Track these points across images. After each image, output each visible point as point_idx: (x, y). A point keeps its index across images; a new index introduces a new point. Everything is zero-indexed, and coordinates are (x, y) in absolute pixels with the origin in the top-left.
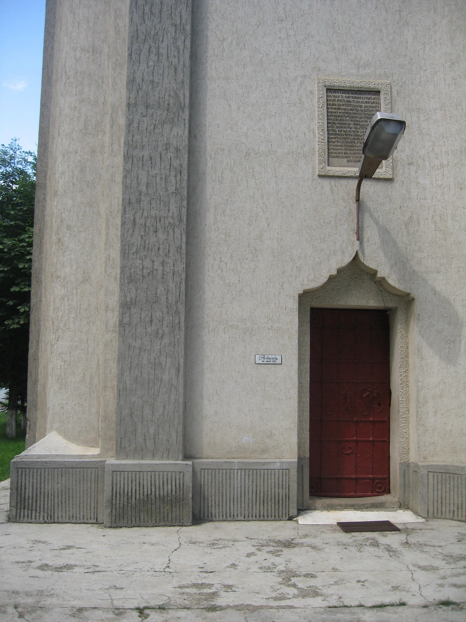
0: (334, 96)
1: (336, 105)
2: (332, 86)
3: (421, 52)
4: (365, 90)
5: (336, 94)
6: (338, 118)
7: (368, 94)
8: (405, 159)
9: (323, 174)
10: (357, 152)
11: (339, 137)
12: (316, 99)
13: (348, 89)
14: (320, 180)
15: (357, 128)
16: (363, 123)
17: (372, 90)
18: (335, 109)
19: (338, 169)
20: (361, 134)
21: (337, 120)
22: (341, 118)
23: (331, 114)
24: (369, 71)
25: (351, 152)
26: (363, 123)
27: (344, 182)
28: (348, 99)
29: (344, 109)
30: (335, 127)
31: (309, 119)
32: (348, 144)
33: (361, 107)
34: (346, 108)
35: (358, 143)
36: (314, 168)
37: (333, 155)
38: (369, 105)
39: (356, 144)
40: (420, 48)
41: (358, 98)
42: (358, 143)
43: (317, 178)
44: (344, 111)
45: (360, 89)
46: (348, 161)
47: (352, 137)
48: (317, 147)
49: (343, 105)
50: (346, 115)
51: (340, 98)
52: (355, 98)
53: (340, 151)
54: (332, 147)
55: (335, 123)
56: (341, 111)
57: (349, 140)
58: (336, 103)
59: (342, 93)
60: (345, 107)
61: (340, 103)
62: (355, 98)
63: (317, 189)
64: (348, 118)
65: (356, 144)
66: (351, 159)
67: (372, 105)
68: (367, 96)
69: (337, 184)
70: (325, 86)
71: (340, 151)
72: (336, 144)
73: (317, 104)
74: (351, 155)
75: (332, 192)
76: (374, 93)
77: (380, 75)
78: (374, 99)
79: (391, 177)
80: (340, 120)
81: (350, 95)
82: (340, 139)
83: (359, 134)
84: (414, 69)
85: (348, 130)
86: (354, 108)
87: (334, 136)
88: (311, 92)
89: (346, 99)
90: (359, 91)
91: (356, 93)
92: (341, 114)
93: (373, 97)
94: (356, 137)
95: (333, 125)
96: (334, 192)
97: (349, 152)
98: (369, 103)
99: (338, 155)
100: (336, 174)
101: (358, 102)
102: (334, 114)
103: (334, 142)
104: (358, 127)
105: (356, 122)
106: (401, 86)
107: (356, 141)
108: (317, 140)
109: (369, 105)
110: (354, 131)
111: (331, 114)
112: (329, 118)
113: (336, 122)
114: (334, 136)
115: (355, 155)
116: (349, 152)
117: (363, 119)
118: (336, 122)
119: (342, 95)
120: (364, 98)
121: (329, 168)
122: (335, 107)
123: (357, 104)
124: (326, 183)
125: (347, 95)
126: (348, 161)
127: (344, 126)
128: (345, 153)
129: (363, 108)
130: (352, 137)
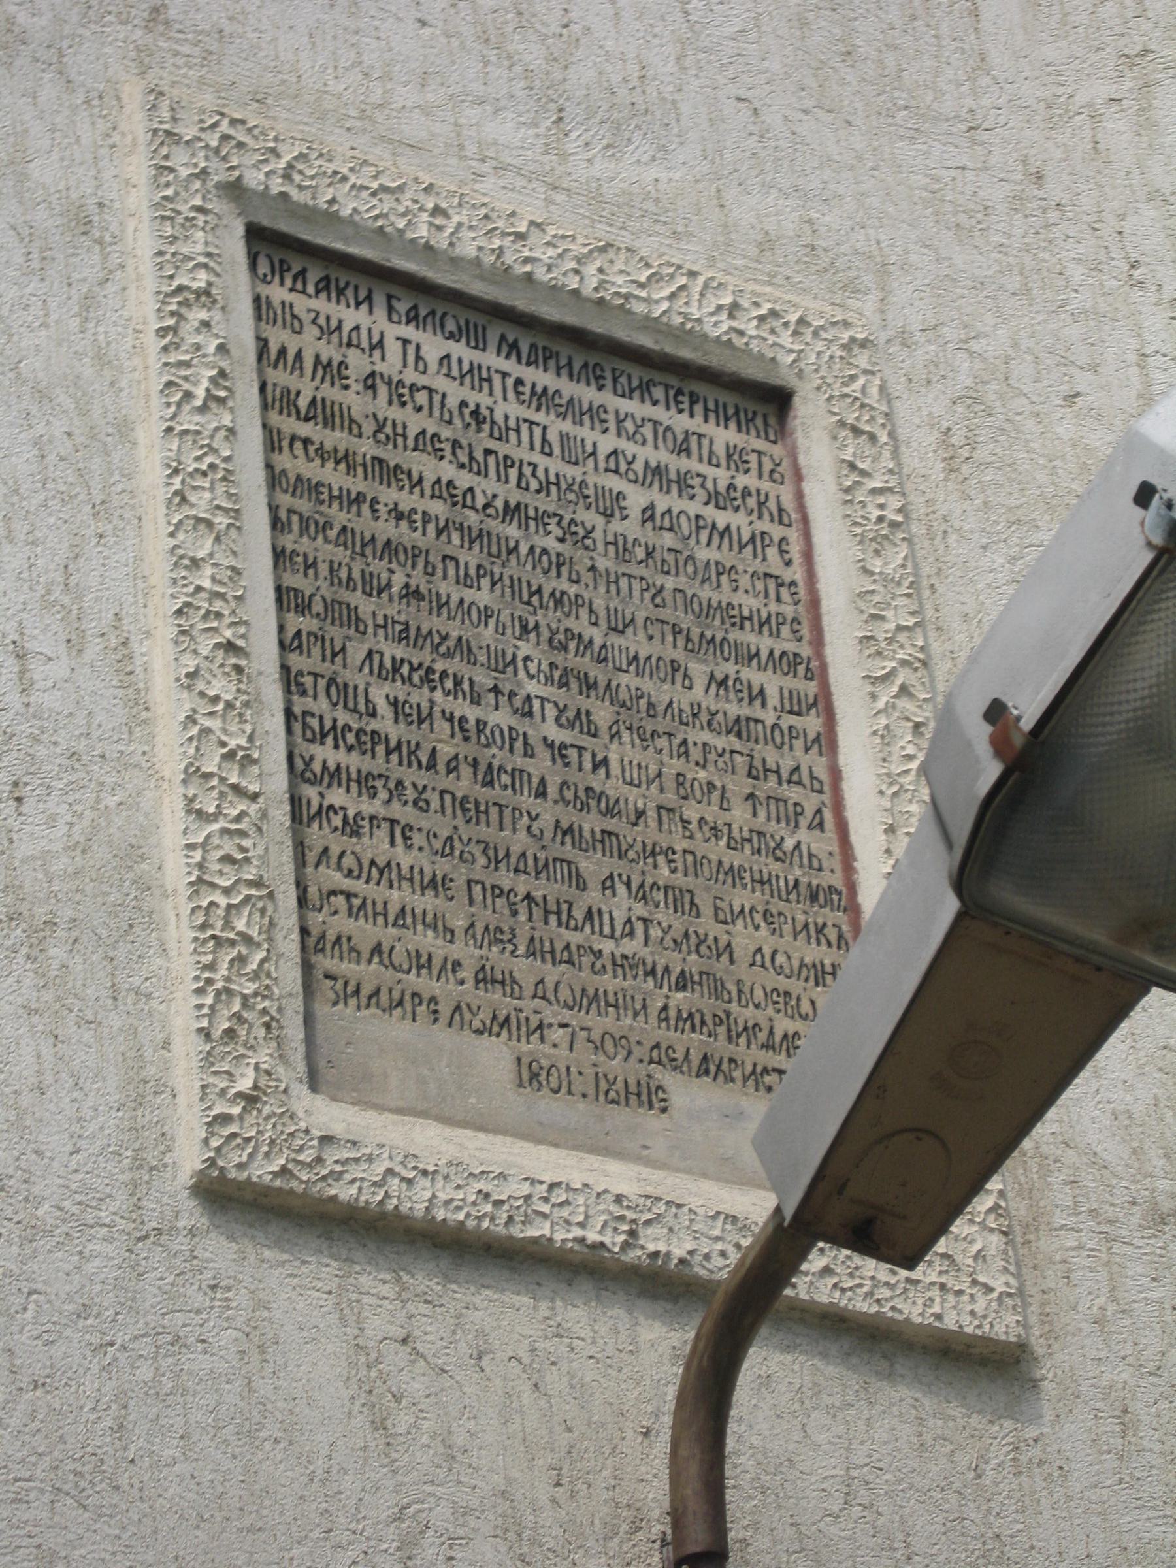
0: (329, 330)
1: (352, 425)
2: (309, 214)
3: (1117, 129)
4: (645, 341)
5: (352, 316)
6: (379, 567)
7: (674, 399)
8: (1113, 1151)
9: (263, 1171)
10: (609, 983)
11: (412, 776)
12: (142, 304)
13: (477, 288)
14: (221, 1251)
15: (581, 720)
16: (647, 685)
17: (714, 359)
18: (345, 459)
19: (431, 1141)
20: (634, 798)
21: (375, 588)
22: (418, 579)
23: (304, 505)
24: (653, 172)
25: (553, 973)
26: (647, 685)
27: (508, 1315)
28: (473, 398)
29: (445, 490)
30: (357, 652)
31: (67, 499)
32: (505, 879)
33: (612, 507)
34: (464, 479)
35: (608, 884)
36: (143, 1091)
37: (346, 968)
38: (693, 508)
39: (593, 896)
40: (1106, 90)
41: (571, 410)
42: (608, 884)
43: (191, 1214)
44: (438, 508)
45: (596, 325)
46: (531, 1075)
47: (548, 814)
48: (172, 832)
49: (427, 442)
50: (471, 558)
51: (391, 363)
52: (542, 398)
53: (428, 941)
54: (337, 879)
55: (353, 619)
56: (408, 500)
57: (520, 841)
58: (355, 401)
59: (412, 318)
60: (448, 471)
61: (395, 413)
62: (542, 398)
63: (197, 1362)
64: (483, 596)
65: (593, 896)
66: (553, 1049)
67: (722, 519)
68: (660, 413)
69: (431, 1332)
70: (235, 190)
71: (428, 941)
72: (375, 846)
73: (154, 359)
74: (550, 1014)
75: (380, 1425)
76: (730, 399)
77: (767, 244)
78: (735, 458)
79: (1004, 1327)
80: (411, 594)
81: (491, 359)
82: (420, 804)
83: (614, 788)
84: (1077, 273)
85: (501, 718)
86: (547, 504)
87: (354, 762)
88: (83, 223)
89: (455, 393)
90: (578, 337)
91: (540, 357)
92: (402, 533)
93: (724, 436)
94: (591, 823)
95: (335, 633)
96: (402, 1421)
97: (525, 969)
98: (682, 483)
99: (414, 980)
100: (415, 1201)
101: (571, 452)
102: (339, 516)
103: (351, 827)
104: (603, 714)
105: (571, 659)
106: (972, 398)
107: (592, 865)
108: (172, 764)
109: (693, 508)
110: (559, 752)
111: (304, 505)
112: (288, 542)
113: (365, 606)
114: (354, 762)
115: (601, 1022)
116: (525, 969)
117: (636, 643)
118: (365, 606)
119: (409, 331)
120: (630, 429)
121: (324, 1114)
122: (335, 438)
123: (572, 472)
124: (299, 1289)
125: (460, 350)
126: (531, 1075)
127: (454, 665)
128: (484, 978)
129: (631, 528)
130: (548, 814)
